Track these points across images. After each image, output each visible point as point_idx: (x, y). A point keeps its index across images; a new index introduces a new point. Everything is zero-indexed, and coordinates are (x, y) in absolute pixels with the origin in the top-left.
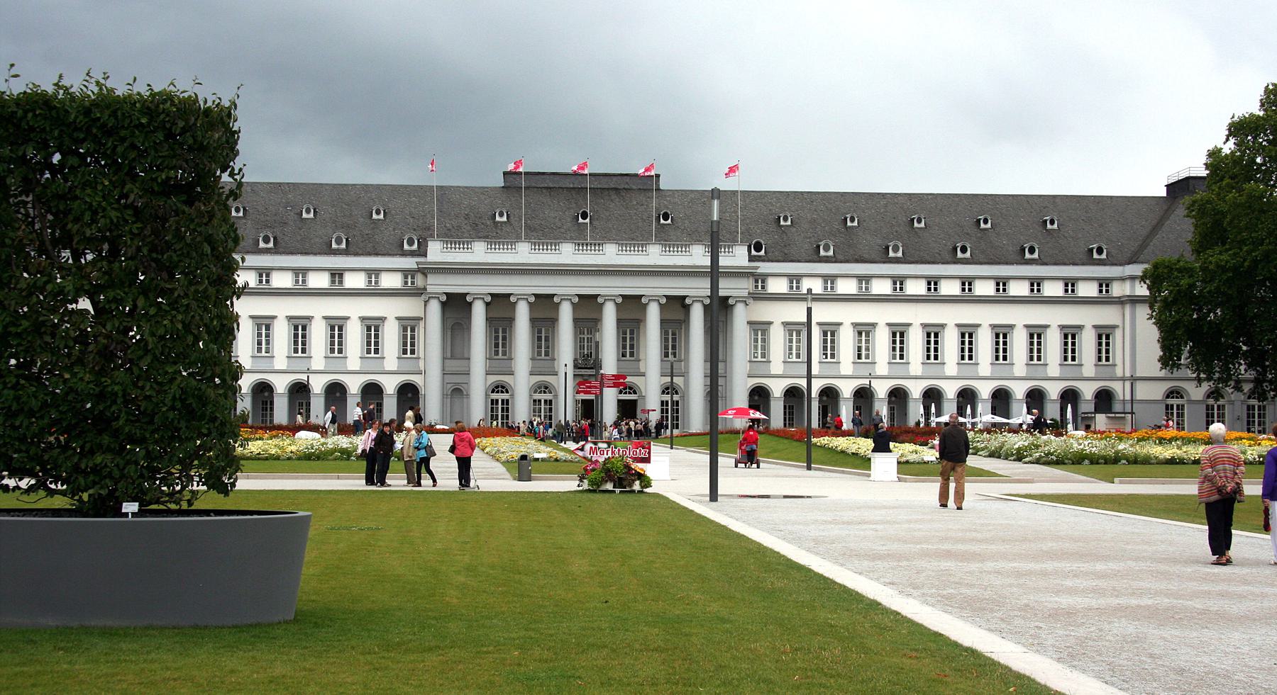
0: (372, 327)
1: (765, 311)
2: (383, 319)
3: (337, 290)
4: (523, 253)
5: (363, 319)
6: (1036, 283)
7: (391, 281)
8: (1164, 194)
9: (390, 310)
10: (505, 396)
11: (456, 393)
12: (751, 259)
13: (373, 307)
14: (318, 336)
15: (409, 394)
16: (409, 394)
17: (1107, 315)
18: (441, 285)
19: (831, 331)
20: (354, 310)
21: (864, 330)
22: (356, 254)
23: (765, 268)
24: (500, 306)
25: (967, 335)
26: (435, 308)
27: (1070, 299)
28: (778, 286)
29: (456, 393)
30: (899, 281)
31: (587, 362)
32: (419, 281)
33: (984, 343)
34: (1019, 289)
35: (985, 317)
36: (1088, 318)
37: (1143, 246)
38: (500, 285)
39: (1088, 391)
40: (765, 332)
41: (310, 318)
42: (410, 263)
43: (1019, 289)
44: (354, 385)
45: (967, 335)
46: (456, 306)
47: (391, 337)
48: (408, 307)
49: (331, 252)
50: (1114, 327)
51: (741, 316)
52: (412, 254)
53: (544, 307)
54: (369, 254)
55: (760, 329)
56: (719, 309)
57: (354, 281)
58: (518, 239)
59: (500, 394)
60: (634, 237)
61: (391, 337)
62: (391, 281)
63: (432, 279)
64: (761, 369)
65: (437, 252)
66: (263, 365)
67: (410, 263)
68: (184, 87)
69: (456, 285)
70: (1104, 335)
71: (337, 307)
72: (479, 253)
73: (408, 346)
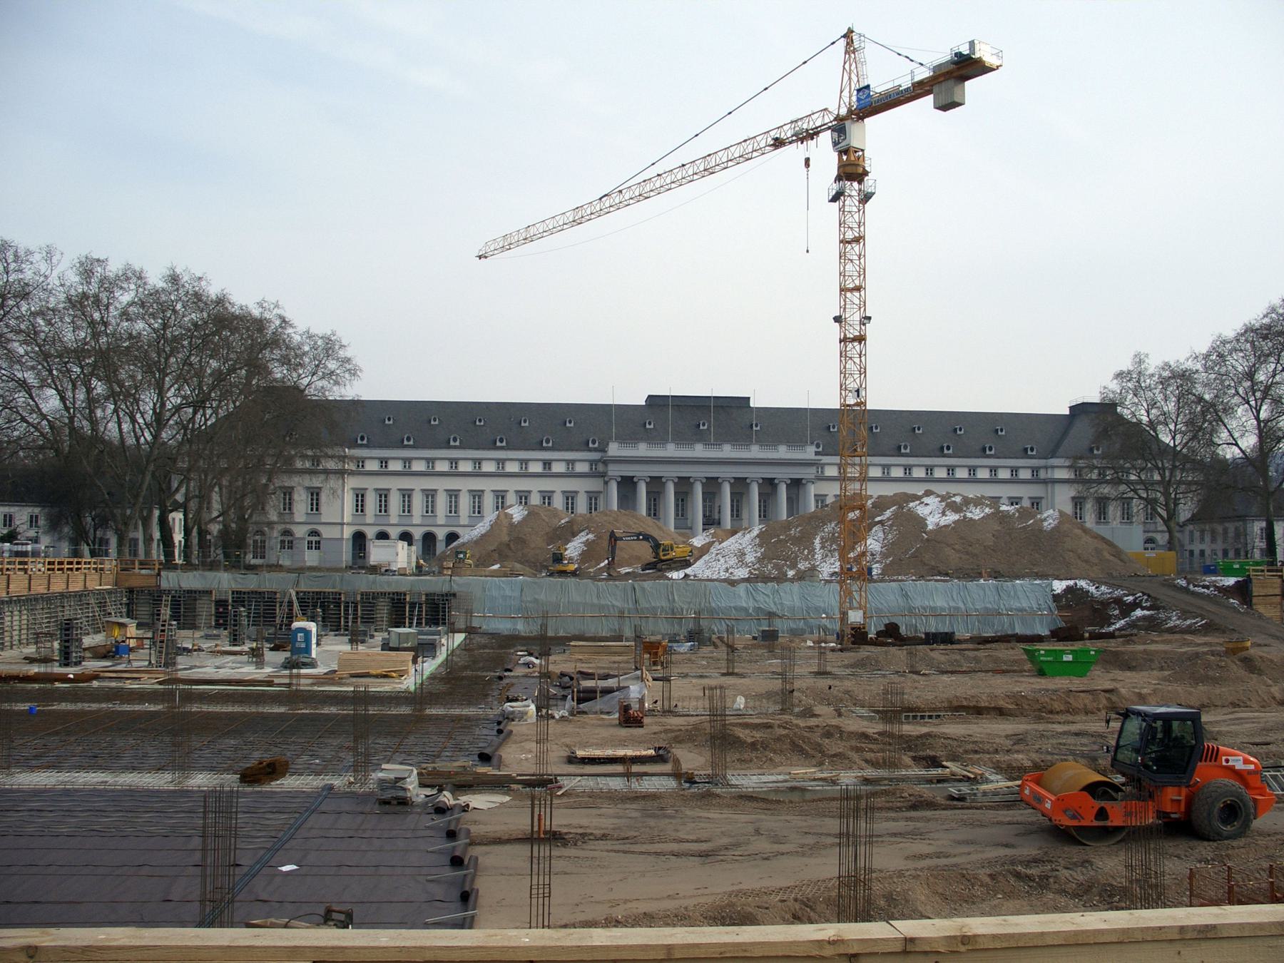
2: (576, 492)
4: (671, 450)
5: (564, 492)
6: (951, 469)
7: (582, 468)
8: (1067, 413)
10: (290, 538)
12: (817, 453)
13: (571, 484)
14: (395, 502)
17: (1036, 491)
18: (615, 471)
22: (559, 450)
23: (825, 459)
26: (614, 487)
30: (908, 468)
32: (601, 468)
37: (1058, 445)
38: (656, 471)
40: (456, 496)
41: (529, 492)
42: (595, 456)
46: (627, 484)
49: (449, 447)
50: (1041, 498)
52: (595, 450)
53: (684, 486)
54: (567, 450)
56: (796, 485)
57: (558, 468)
58: (751, 443)
62: (582, 468)
64: (287, 518)
65: (614, 449)
66: (405, 521)
67: (595, 456)
68: (305, 314)
69: (628, 471)
72: (643, 450)
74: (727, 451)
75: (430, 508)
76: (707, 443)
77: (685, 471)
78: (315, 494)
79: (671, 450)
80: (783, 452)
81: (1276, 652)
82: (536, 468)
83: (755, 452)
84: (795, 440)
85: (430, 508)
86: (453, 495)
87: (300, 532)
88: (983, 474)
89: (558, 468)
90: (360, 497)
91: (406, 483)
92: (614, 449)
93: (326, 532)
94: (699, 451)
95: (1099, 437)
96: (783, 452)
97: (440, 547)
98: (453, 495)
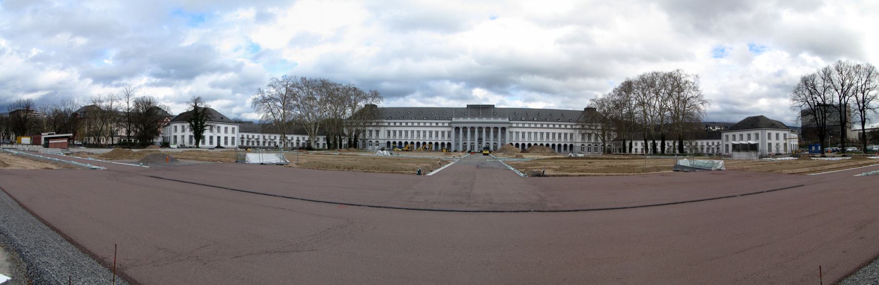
0: (443, 133)
1: (512, 130)
3: (437, 126)
4: (469, 120)
7: (446, 125)
9: (446, 130)
11: (457, 144)
13: (443, 129)
14: (403, 133)
15: (449, 144)
16: (449, 144)
17: (572, 131)
18: (454, 125)
19: (517, 133)
20: (440, 130)
21: (530, 133)
24: (465, 128)
25: (548, 134)
27: (566, 128)
28: (514, 125)
29: (457, 144)
31: (480, 140)
33: (551, 136)
34: (557, 126)
35: (551, 131)
36: (569, 132)
38: (465, 125)
39: (545, 144)
43: (557, 126)
44: (440, 143)
45: (548, 134)
46: (457, 129)
47: (446, 134)
48: (449, 129)
51: (507, 131)
53: (473, 129)
55: (511, 133)
56: (504, 129)
59: (495, 144)
60: (488, 116)
61: (446, 134)
62: (446, 125)
63: (763, 133)
65: (454, 120)
69: (457, 125)
70: (571, 135)
71: (407, 129)
72: (461, 120)
73: (449, 136)
74: (484, 120)
75: (407, 135)
76: (479, 117)
77: (480, 125)
78: (377, 132)
79: (469, 120)
80: (500, 120)
81: (875, 148)
82: (434, 125)
83: (492, 120)
84: (504, 117)
85: (407, 135)
86: (418, 132)
87: (374, 141)
88: (545, 126)
89: (440, 125)
90: (389, 132)
91: (419, 129)
92: (454, 120)
93: (380, 141)
94: (477, 120)
95: (589, 117)
96: (500, 120)
97: (392, 145)
98: (418, 132)
